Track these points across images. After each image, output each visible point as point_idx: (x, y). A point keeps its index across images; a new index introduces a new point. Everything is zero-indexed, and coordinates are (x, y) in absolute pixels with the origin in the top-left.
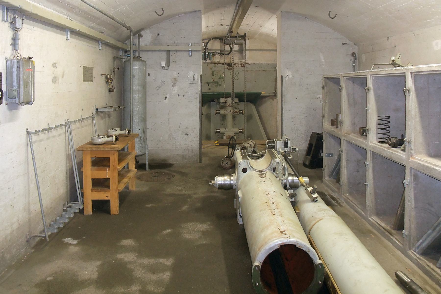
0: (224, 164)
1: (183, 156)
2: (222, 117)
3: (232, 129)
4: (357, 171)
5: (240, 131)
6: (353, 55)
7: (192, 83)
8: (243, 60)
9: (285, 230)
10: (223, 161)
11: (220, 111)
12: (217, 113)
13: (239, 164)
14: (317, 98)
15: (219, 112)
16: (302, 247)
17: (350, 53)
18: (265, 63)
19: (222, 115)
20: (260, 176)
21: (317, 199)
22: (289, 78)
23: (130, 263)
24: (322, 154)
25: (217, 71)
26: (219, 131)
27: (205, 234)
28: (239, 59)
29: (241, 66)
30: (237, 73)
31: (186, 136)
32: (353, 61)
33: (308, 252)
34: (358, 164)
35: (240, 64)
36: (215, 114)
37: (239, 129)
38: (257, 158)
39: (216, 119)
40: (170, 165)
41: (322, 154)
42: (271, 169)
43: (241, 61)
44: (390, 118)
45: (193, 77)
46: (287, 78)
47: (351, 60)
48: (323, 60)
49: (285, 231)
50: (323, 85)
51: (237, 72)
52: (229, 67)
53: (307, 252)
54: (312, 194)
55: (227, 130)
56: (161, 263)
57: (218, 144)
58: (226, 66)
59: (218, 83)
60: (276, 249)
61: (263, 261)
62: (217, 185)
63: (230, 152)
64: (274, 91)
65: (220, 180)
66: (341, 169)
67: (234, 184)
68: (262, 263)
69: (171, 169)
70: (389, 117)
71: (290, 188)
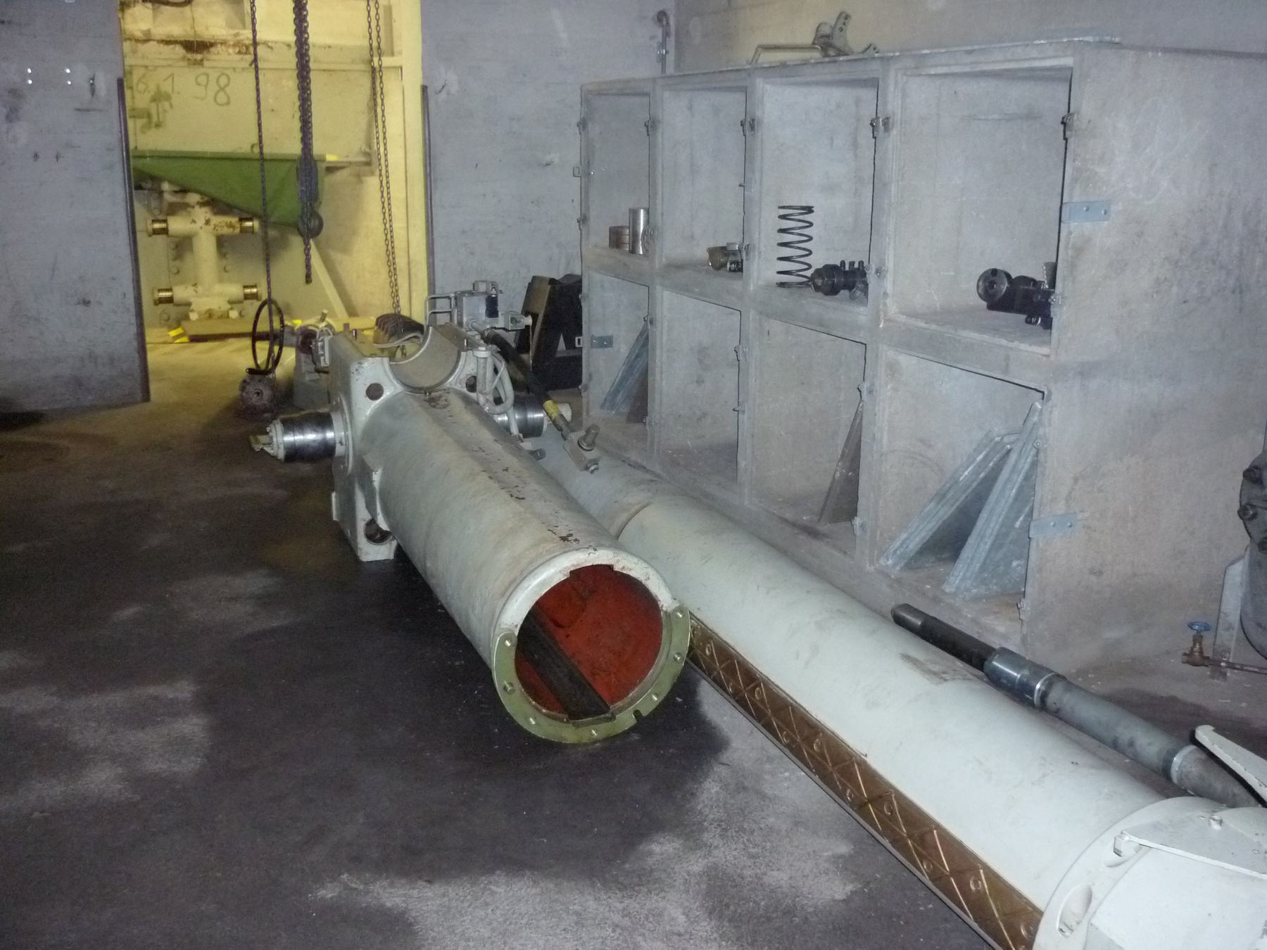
0: (247, 393)
1: (78, 383)
2: (173, 246)
3: (218, 288)
4: (697, 382)
5: (248, 291)
6: (660, 20)
7: (88, 110)
8: (244, 27)
9: (571, 532)
10: (248, 383)
11: (165, 221)
12: (156, 232)
13: (355, 373)
14: (544, 162)
15: (163, 225)
16: (631, 570)
17: (652, 13)
18: (329, 41)
19: (173, 236)
20: (430, 404)
21: (597, 464)
22: (448, 93)
23: (43, 713)
24: (579, 340)
25: (142, 71)
26: (168, 294)
27: (265, 601)
28: (230, 26)
29: (240, 52)
30: (223, 81)
31: (81, 308)
32: (660, 39)
33: (646, 580)
34: (700, 361)
35: (234, 45)
36: (150, 236)
37: (245, 287)
38: (792, 231)
39: (154, 251)
40: (31, 419)
41: (579, 340)
42: (460, 383)
43: (237, 35)
44: (812, 211)
45: (87, 86)
46: (443, 95)
47: (652, 38)
48: (564, 35)
49: (571, 535)
50: (582, 116)
51: (223, 74)
52: (189, 56)
53: (644, 582)
54: (583, 452)
55: (200, 289)
56: (156, 698)
57: (185, 339)
58: (179, 50)
59: (149, 116)
60: (558, 582)
61: (521, 622)
62: (279, 448)
63: (262, 357)
64: (364, 148)
65: (282, 439)
66: (650, 379)
67: (337, 441)
68: (519, 626)
69: (42, 428)
70: (809, 210)
71: (521, 435)
